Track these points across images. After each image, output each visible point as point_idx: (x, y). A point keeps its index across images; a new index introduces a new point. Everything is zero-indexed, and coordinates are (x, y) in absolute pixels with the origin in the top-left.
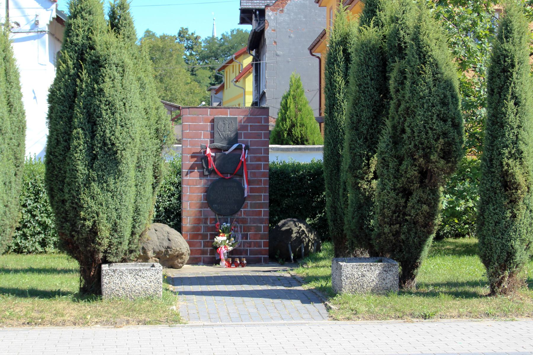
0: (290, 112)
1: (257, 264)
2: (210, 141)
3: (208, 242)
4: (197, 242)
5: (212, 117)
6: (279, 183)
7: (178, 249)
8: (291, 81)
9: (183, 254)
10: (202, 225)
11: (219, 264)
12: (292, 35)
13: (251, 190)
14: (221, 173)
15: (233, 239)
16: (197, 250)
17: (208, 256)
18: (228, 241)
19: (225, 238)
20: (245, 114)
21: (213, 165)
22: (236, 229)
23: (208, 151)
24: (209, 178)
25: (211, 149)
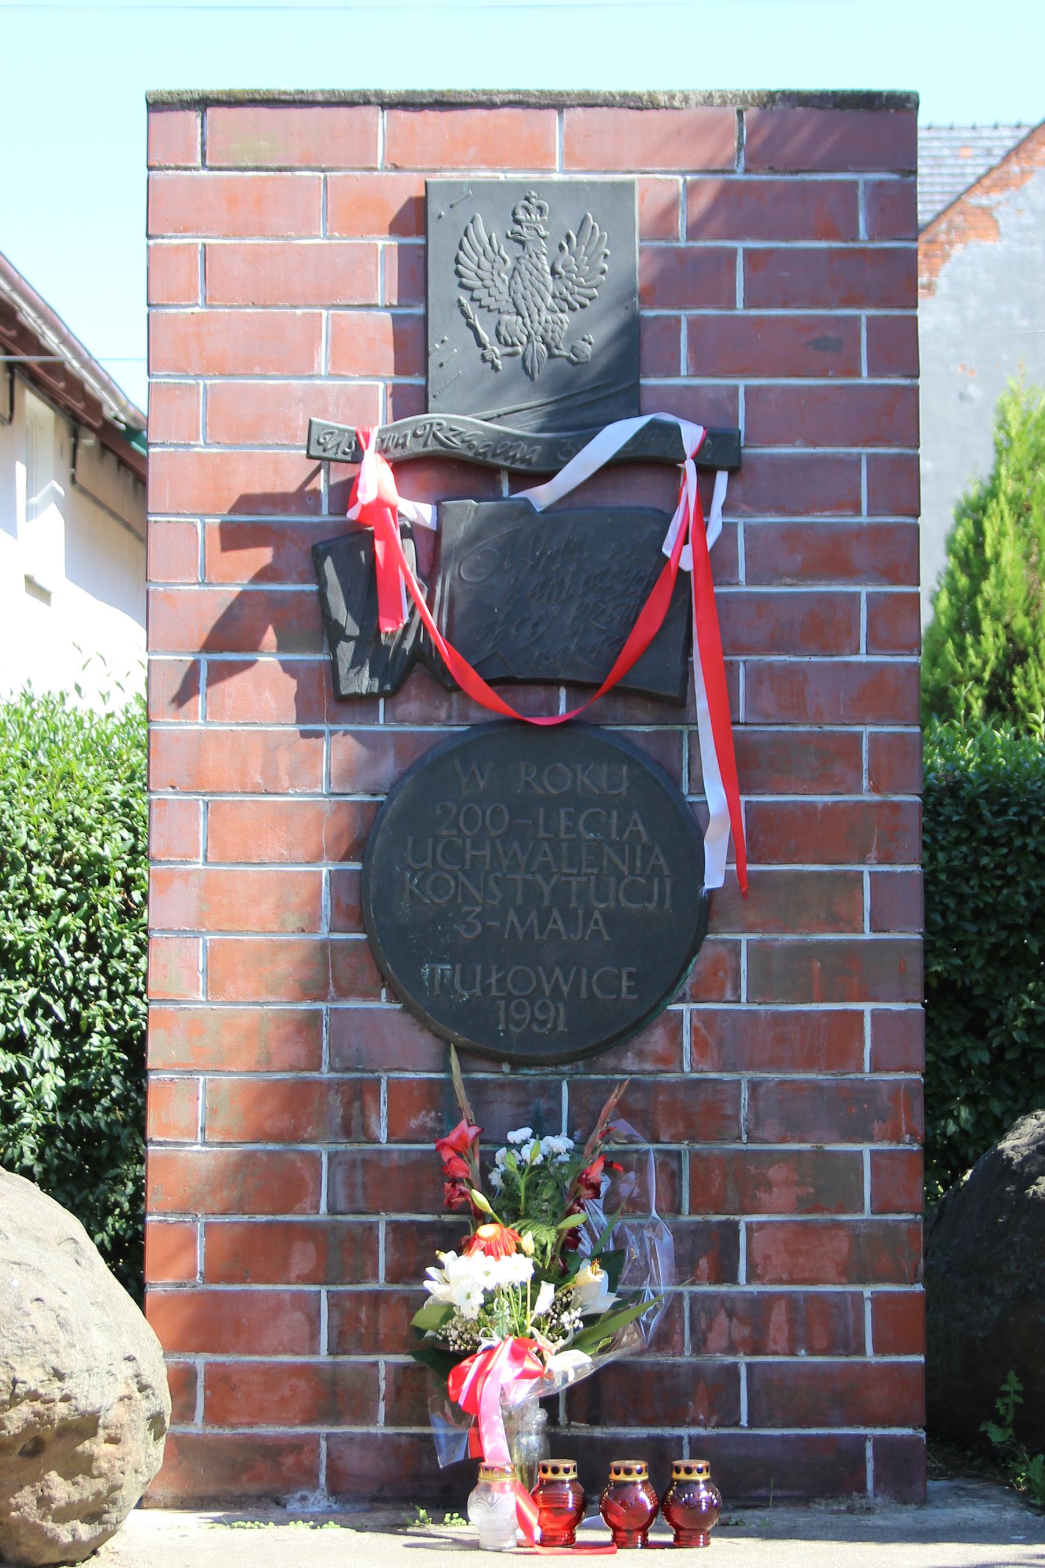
0: (1000, 584)
1: (819, 1513)
2: (398, 394)
3: (376, 1299)
4: (276, 1307)
5: (410, 185)
6: (976, 867)
7: (31, 1377)
8: (1003, 425)
9: (87, 1425)
10: (323, 1150)
11: (460, 1507)
12: (973, 390)
13: (755, 837)
14: (491, 683)
15: (591, 1276)
16: (273, 1375)
17: (380, 1428)
18: (547, 1292)
19: (519, 1269)
20: (703, 153)
21: (416, 608)
22: (627, 1187)
23: (376, 479)
24: (381, 725)
25: (398, 467)
